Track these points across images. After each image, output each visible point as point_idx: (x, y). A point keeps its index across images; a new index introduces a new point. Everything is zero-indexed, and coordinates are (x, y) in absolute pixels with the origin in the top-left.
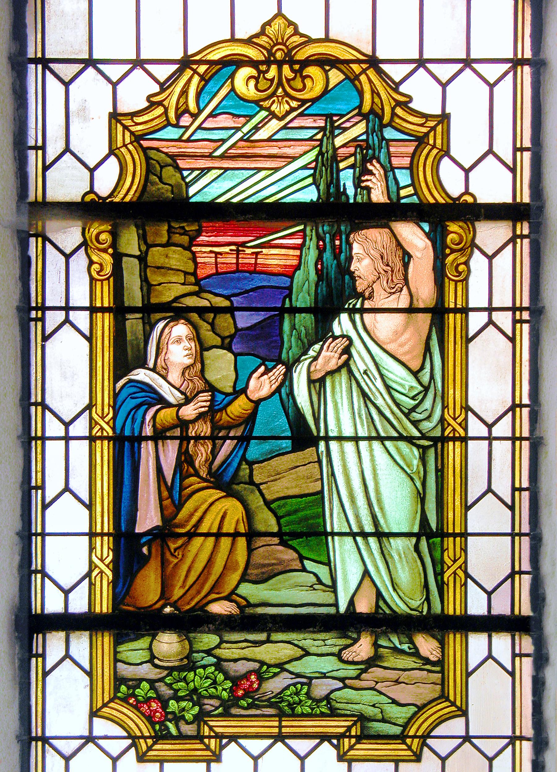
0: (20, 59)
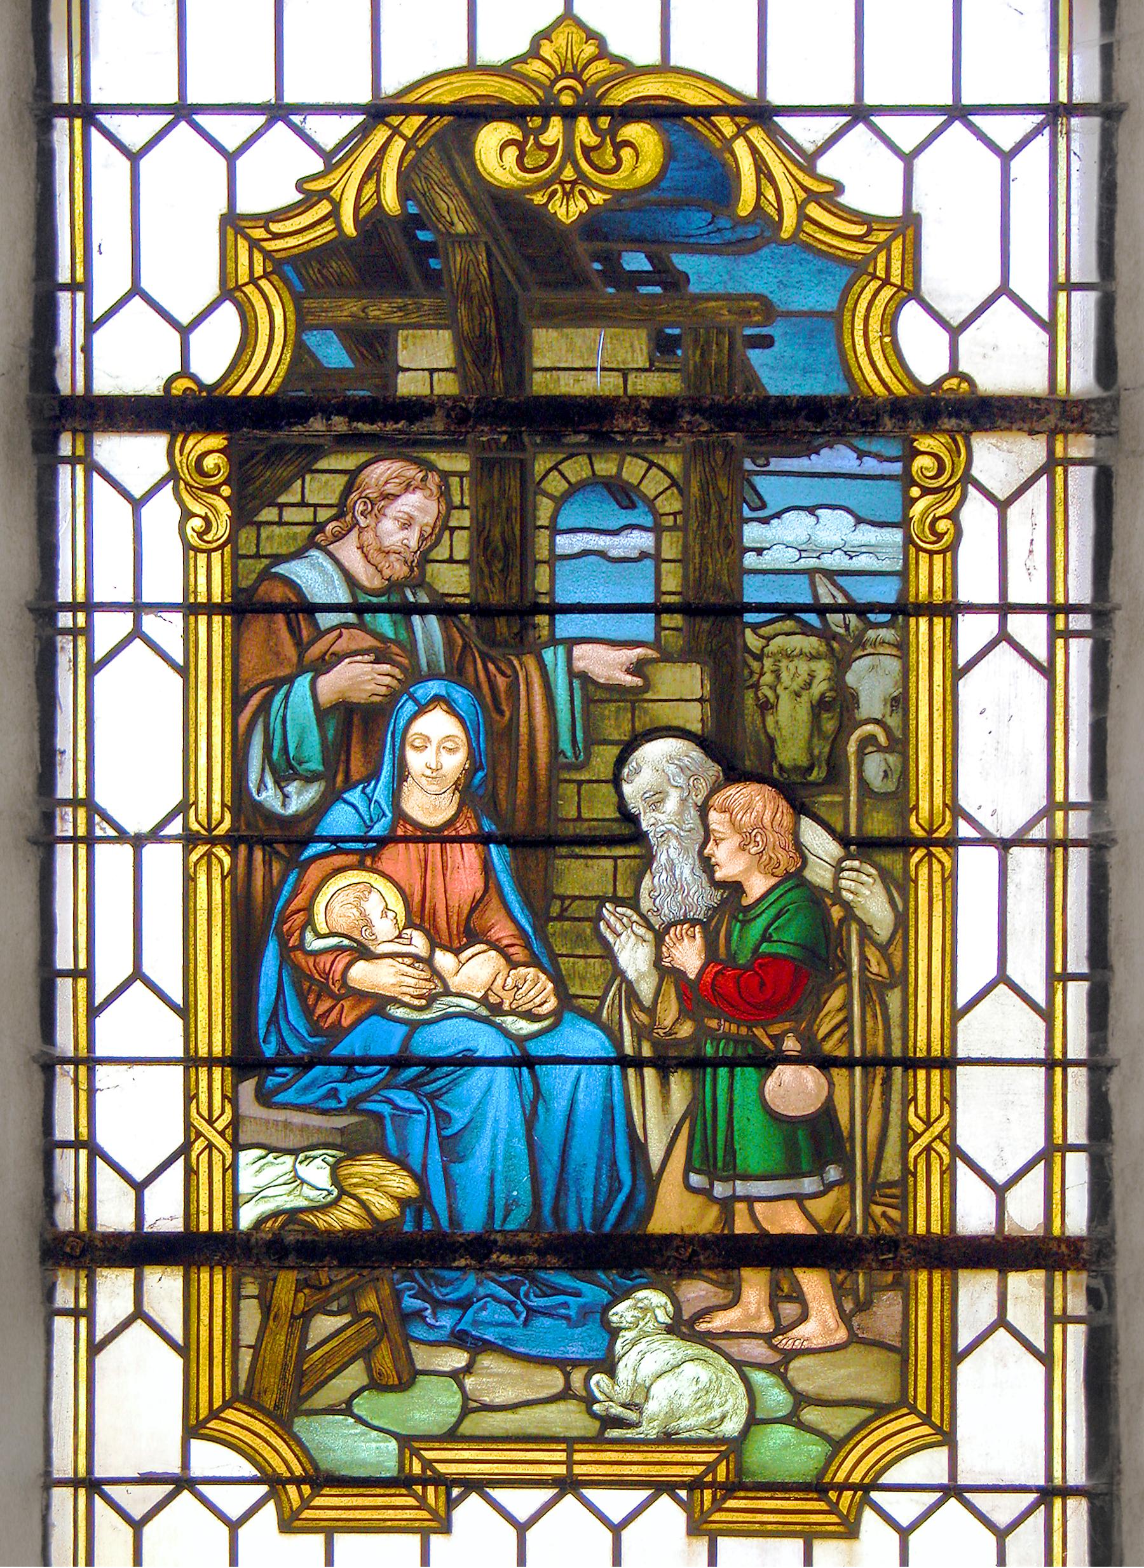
0: (45, 605)
